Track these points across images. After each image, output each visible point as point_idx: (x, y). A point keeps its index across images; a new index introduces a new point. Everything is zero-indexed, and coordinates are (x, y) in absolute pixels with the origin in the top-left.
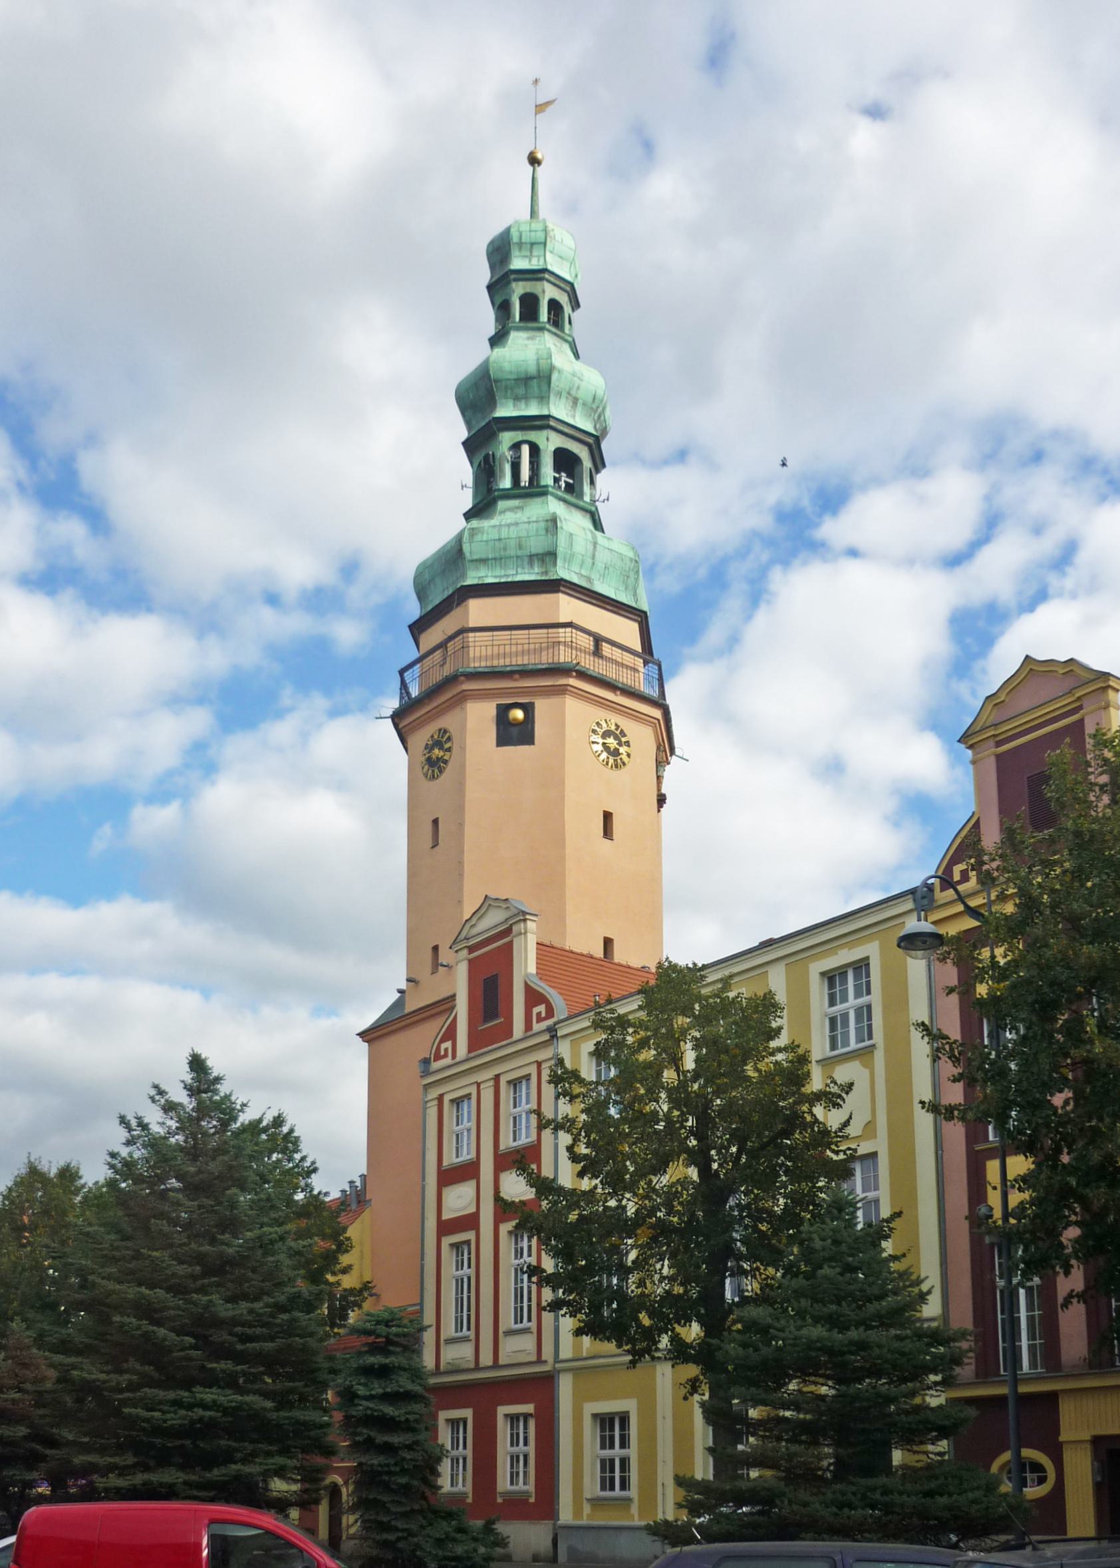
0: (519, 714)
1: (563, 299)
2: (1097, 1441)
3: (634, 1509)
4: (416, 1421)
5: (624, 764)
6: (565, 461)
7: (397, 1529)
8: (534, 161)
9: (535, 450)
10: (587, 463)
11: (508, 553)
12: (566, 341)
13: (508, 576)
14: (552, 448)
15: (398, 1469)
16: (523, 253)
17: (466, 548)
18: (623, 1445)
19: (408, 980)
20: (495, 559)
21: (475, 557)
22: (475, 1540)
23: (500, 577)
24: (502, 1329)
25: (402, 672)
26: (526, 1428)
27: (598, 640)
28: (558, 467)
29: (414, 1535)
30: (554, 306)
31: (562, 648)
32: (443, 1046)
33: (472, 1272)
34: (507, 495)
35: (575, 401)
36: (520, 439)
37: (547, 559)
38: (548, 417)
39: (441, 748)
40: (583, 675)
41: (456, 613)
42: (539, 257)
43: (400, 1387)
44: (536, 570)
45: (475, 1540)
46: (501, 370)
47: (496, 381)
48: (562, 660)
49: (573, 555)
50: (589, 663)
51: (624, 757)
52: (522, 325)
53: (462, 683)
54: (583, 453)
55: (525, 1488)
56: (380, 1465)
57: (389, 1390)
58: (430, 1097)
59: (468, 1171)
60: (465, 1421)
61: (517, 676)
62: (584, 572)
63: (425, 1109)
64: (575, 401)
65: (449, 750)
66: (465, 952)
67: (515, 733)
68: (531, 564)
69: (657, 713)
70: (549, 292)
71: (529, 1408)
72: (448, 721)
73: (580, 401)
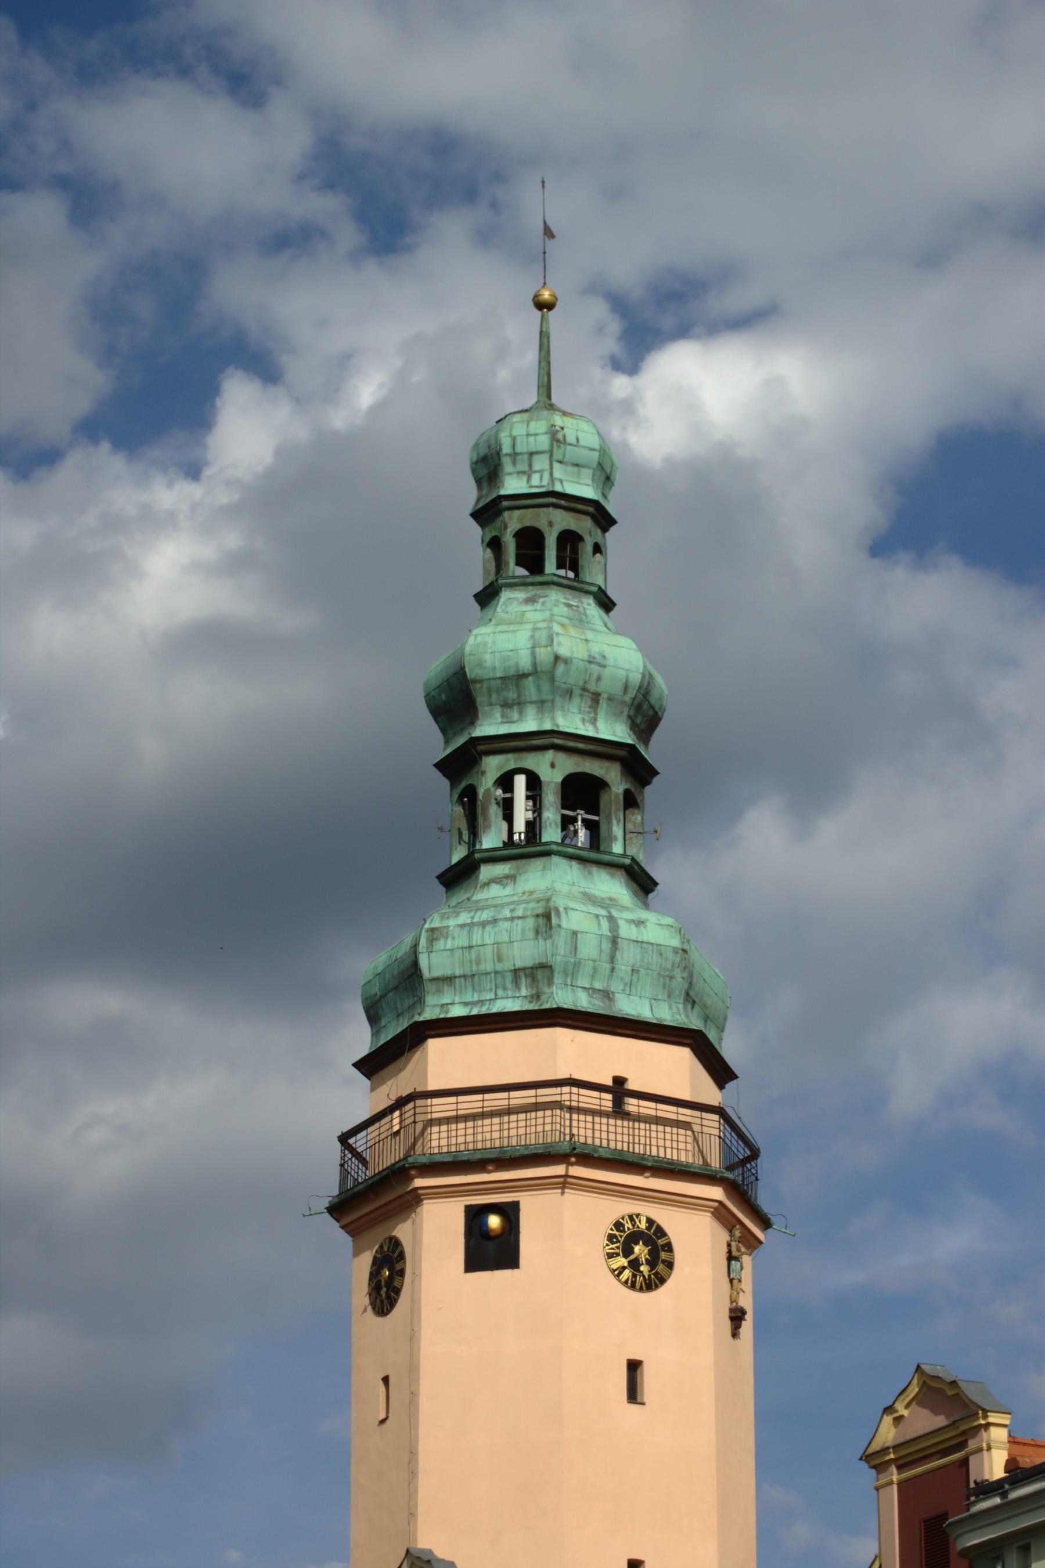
0: (494, 1221)
12: (587, 592)
13: (482, 1002)
17: (423, 961)
20: (465, 976)
21: (436, 974)
23: (473, 1004)
34: (493, 858)
35: (596, 698)
40: (588, 1157)
46: (480, 664)
47: (475, 681)
62: (598, 985)
64: (596, 698)
67: (492, 1246)
70: (554, 523)
72: (402, 1231)
73: (605, 696)
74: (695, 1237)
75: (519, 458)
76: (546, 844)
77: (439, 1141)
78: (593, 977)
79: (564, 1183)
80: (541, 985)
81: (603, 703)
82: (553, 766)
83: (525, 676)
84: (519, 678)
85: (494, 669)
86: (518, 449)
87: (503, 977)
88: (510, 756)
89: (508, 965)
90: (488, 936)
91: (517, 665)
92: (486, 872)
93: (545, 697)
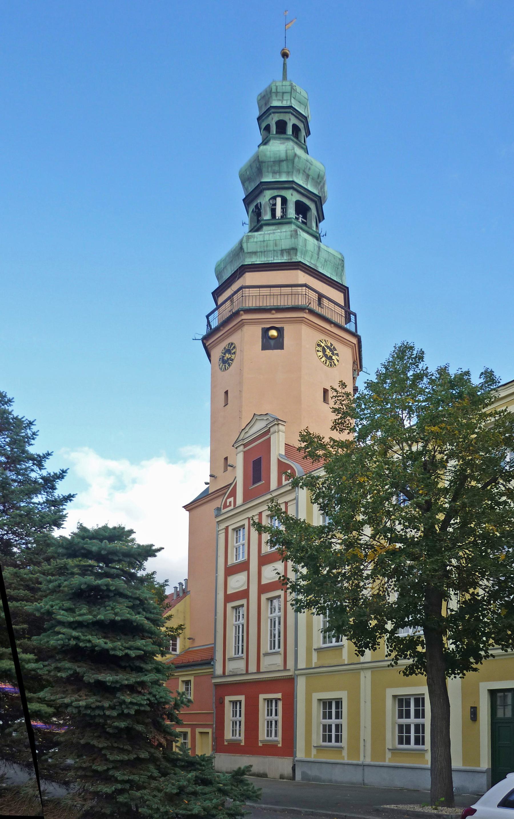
0: (273, 333)
1: (301, 126)
3: (345, 753)
4: (139, 658)
5: (335, 365)
6: (302, 209)
7: (117, 781)
8: (285, 55)
9: (284, 201)
11: (269, 249)
14: (294, 200)
15: (115, 713)
16: (278, 98)
17: (245, 246)
18: (337, 717)
19: (211, 476)
20: (261, 252)
21: (249, 251)
22: (224, 792)
24: (262, 652)
25: (208, 317)
26: (276, 706)
28: (298, 212)
29: (139, 788)
30: (295, 128)
31: (300, 296)
32: (228, 500)
33: (244, 622)
35: (308, 176)
36: (276, 194)
37: (292, 252)
38: (293, 182)
39: (230, 353)
40: (312, 312)
42: (287, 100)
43: (116, 614)
44: (285, 258)
45: (224, 792)
46: (265, 155)
48: (300, 304)
49: (306, 251)
50: (314, 306)
51: (336, 362)
52: (277, 136)
53: (242, 315)
54: (312, 206)
55: (276, 739)
56: (87, 707)
57: (101, 617)
58: (220, 528)
59: (244, 566)
60: (240, 702)
61: (273, 312)
63: (218, 535)
64: (308, 176)
65: (234, 353)
66: (242, 447)
67: (272, 342)
68: (282, 254)
69: (354, 341)
70: (291, 121)
71: (279, 696)
72: (234, 339)
73: (311, 177)
75: (278, 94)
76: (290, 218)
78: (311, 258)
80: (292, 255)
81: (310, 179)
82: (292, 195)
83: (282, 161)
84: (280, 161)
85: (271, 157)
86: (278, 91)
87: (277, 253)
88: (275, 191)
89: (279, 248)
91: (280, 156)
93: (290, 170)
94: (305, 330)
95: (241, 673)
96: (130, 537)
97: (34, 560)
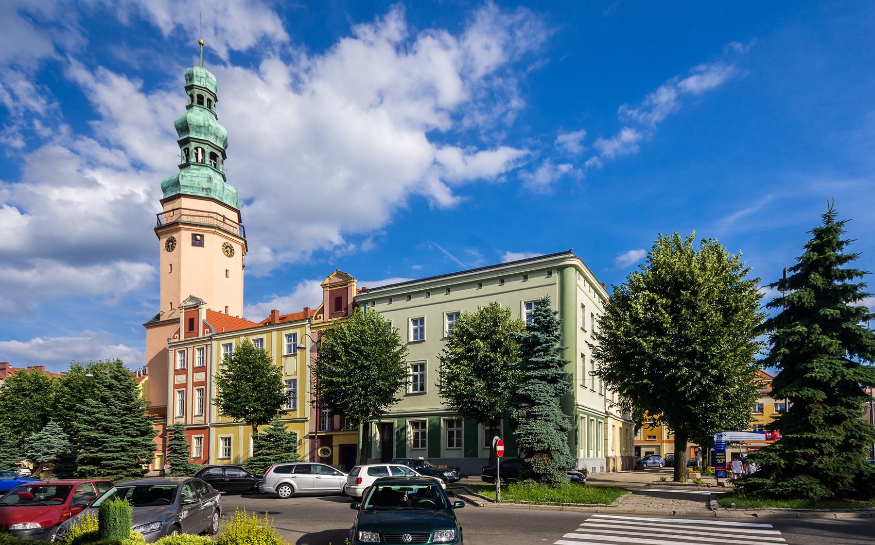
0: (199, 237)
1: (212, 99)
2: (340, 445)
6: (213, 156)
10: (221, 158)
27: (224, 217)
40: (219, 229)
41: (178, 201)
50: (221, 225)
54: (219, 154)
59: (195, 384)
67: (198, 242)
69: (243, 242)
70: (207, 96)
74: (238, 249)
77: (184, 219)
79: (215, 233)
90: (197, 179)
92: (192, 167)
94: (216, 237)
95: (653, 499)
96: (376, 478)
97: (566, 438)
